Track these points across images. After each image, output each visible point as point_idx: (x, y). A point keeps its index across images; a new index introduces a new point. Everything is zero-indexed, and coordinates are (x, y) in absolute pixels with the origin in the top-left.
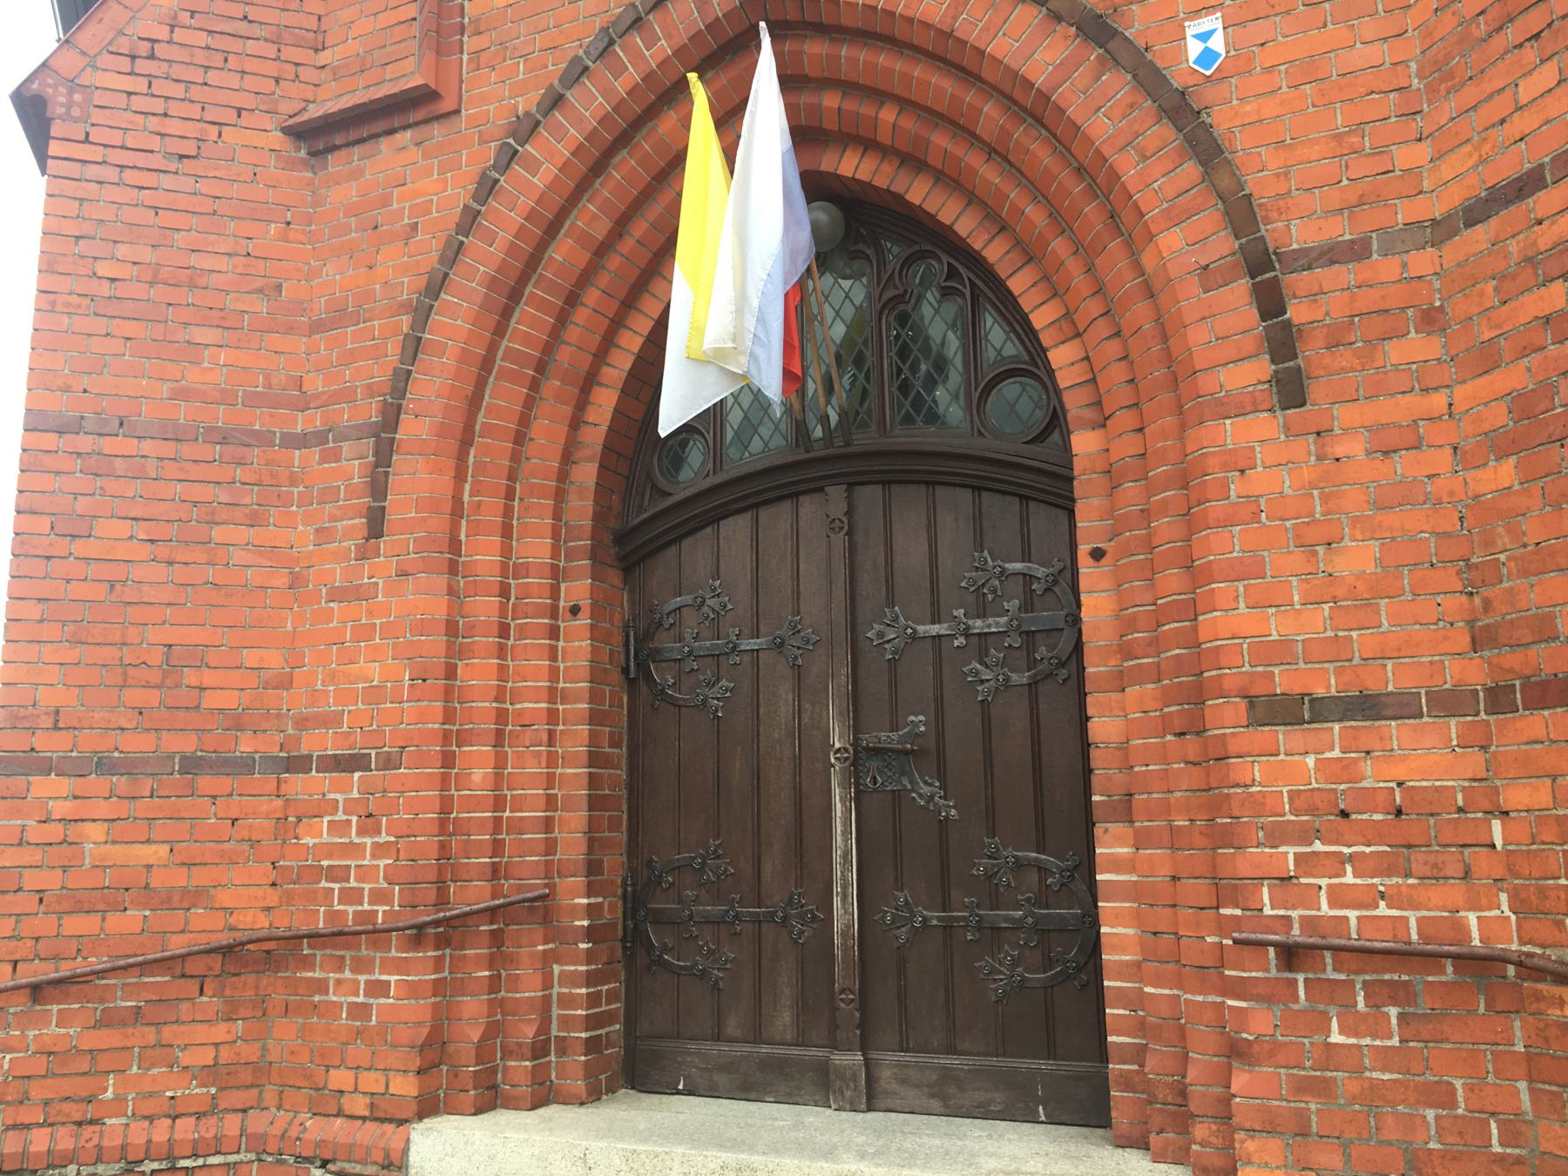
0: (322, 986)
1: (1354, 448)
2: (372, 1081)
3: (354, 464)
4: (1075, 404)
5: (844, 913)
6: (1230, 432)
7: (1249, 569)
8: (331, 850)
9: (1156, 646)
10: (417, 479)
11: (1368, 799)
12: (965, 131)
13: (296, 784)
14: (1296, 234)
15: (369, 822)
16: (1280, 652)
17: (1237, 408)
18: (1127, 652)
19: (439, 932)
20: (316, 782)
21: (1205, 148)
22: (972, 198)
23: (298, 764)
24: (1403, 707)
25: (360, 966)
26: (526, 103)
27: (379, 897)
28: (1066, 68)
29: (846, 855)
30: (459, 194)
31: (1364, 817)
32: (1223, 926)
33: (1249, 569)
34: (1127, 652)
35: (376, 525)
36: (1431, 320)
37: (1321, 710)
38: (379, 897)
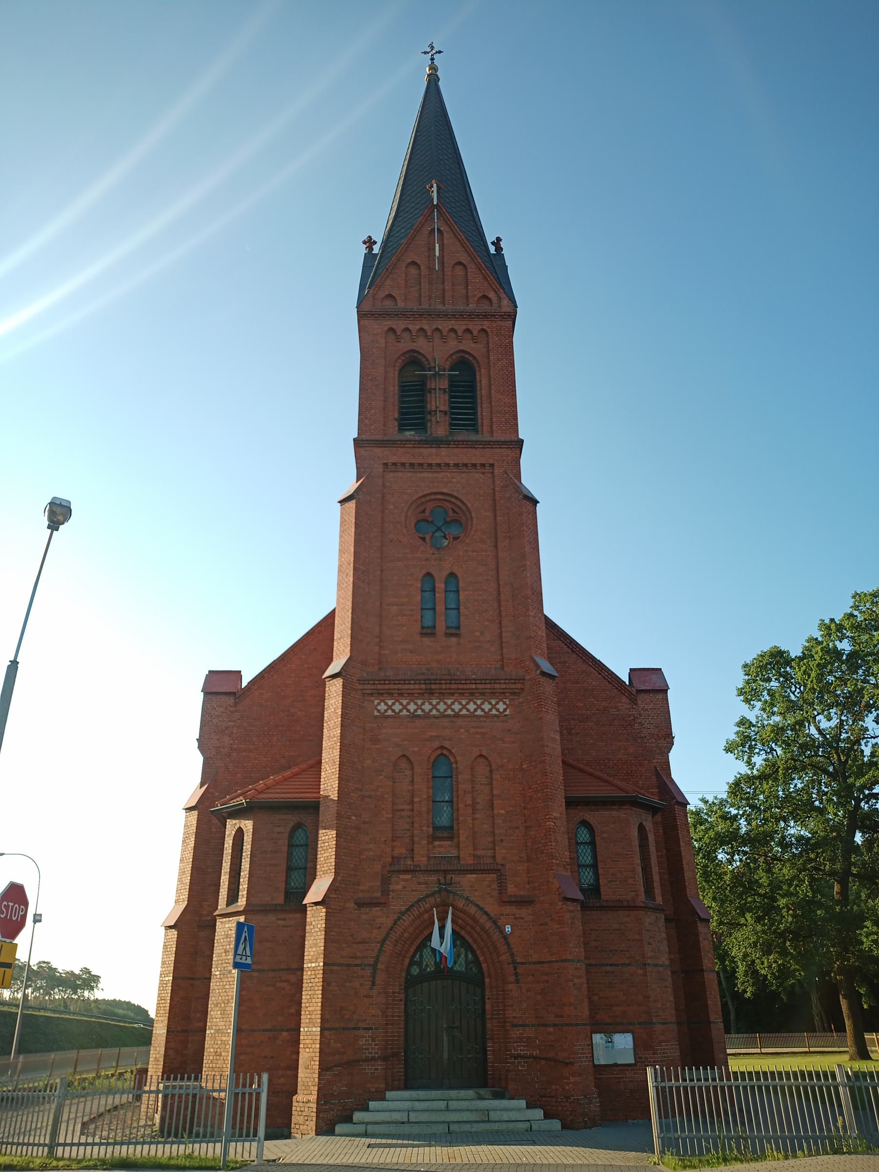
0: (365, 1069)
1: (524, 991)
2: (376, 1086)
3: (368, 972)
4: (486, 974)
5: (446, 1055)
6: (510, 986)
7: (512, 1006)
8: (365, 1045)
9: (498, 1014)
10: (380, 977)
11: (525, 1038)
12: (474, 929)
13: (357, 1032)
14: (519, 959)
15: (373, 1040)
16: (515, 1018)
17: (512, 983)
18: (493, 1015)
19: (385, 1059)
20: (362, 1032)
21: (508, 944)
22: (471, 936)
23: (359, 1029)
24: (528, 1026)
25: (372, 1065)
26: (403, 909)
27: (376, 1053)
28: (490, 928)
29: (156, 1060)
30: (390, 923)
31: (136, 1025)
32: (507, 1055)
33: (512, 1006)
34: (493, 1015)
35: (373, 984)
36: (533, 975)
37: (520, 1026)
38: (376, 1053)
